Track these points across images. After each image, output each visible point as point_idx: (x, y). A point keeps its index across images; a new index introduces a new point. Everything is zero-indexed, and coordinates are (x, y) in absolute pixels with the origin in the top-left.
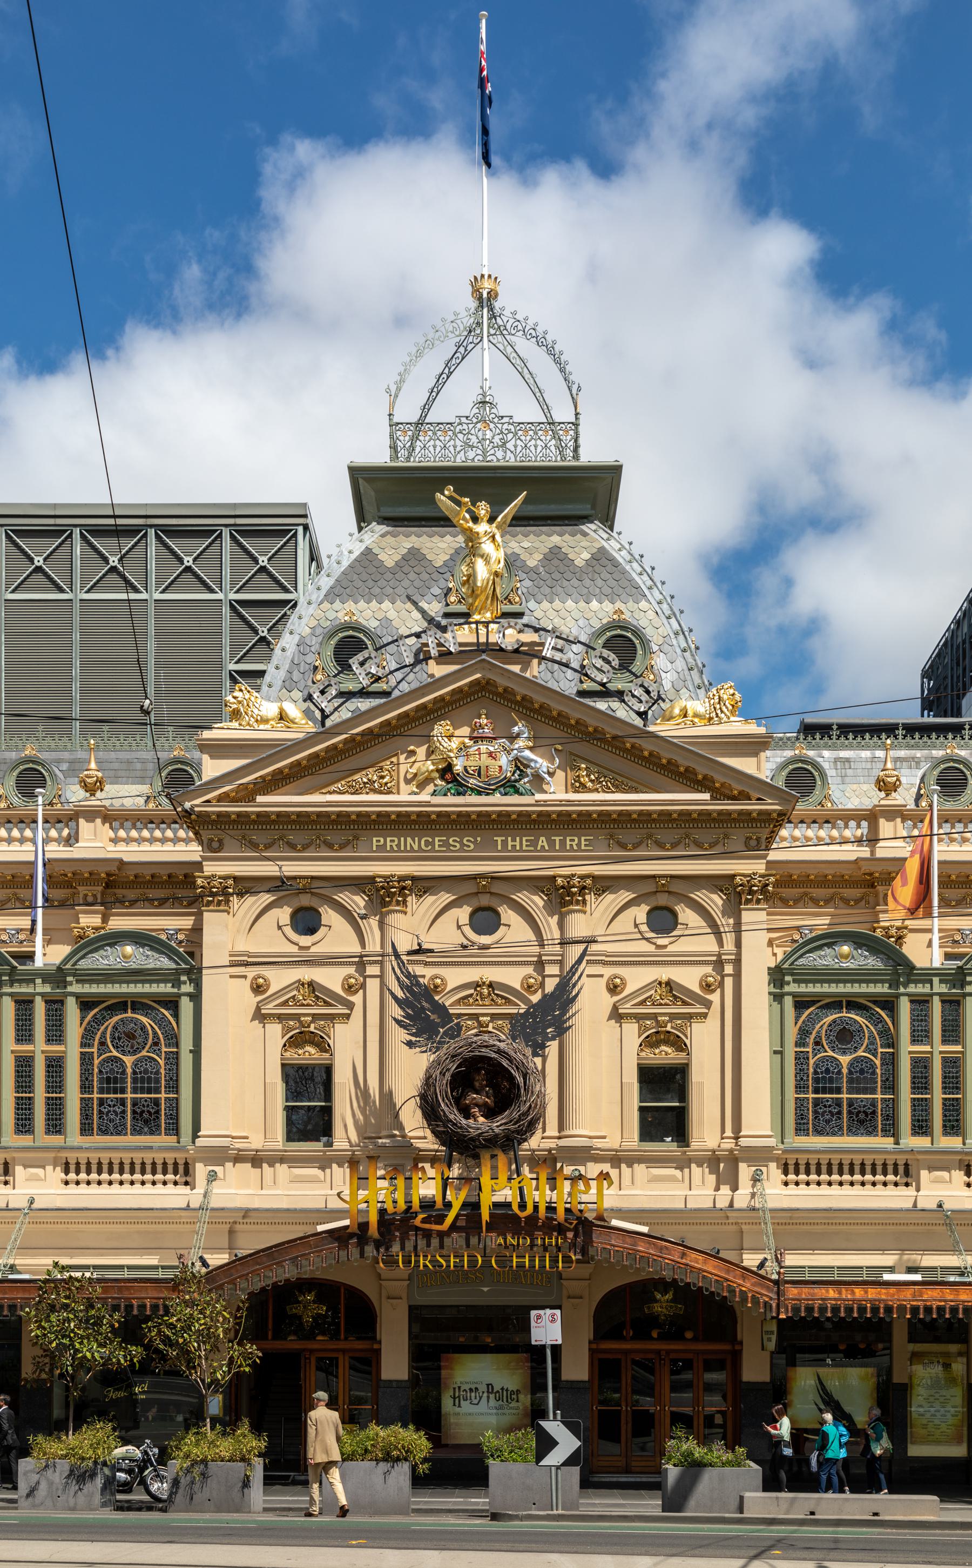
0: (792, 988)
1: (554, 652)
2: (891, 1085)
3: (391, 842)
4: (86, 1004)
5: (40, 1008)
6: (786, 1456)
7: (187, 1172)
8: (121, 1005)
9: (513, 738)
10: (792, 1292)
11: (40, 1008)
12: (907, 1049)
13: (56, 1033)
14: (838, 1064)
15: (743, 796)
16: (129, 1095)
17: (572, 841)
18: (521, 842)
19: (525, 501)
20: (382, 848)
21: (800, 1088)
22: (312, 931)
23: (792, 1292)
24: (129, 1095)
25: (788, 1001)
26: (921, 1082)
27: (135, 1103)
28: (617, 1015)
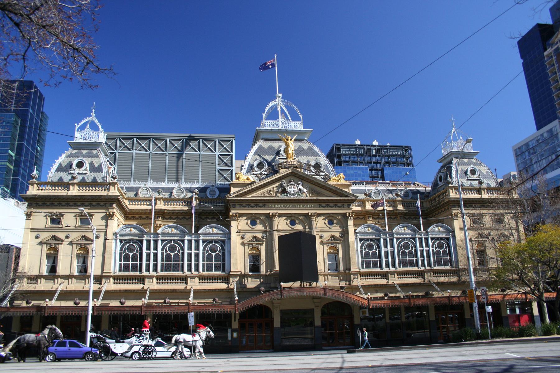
0: (359, 237)
1: (94, 175)
2: (416, 256)
3: (273, 206)
4: (204, 241)
5: (193, 242)
6: (238, 335)
7: (228, 280)
8: (211, 241)
9: (298, 184)
10: (371, 302)
11: (193, 242)
12: (419, 249)
13: (197, 248)
14: (129, 255)
15: (347, 196)
16: (131, 262)
17: (312, 206)
18: (301, 206)
19: (12, 151)
20: (271, 207)
21: (120, 260)
22: (255, 225)
23: (371, 302)
24: (214, 262)
25: (358, 239)
26: (387, 256)
27: (215, 264)
28: (243, 244)
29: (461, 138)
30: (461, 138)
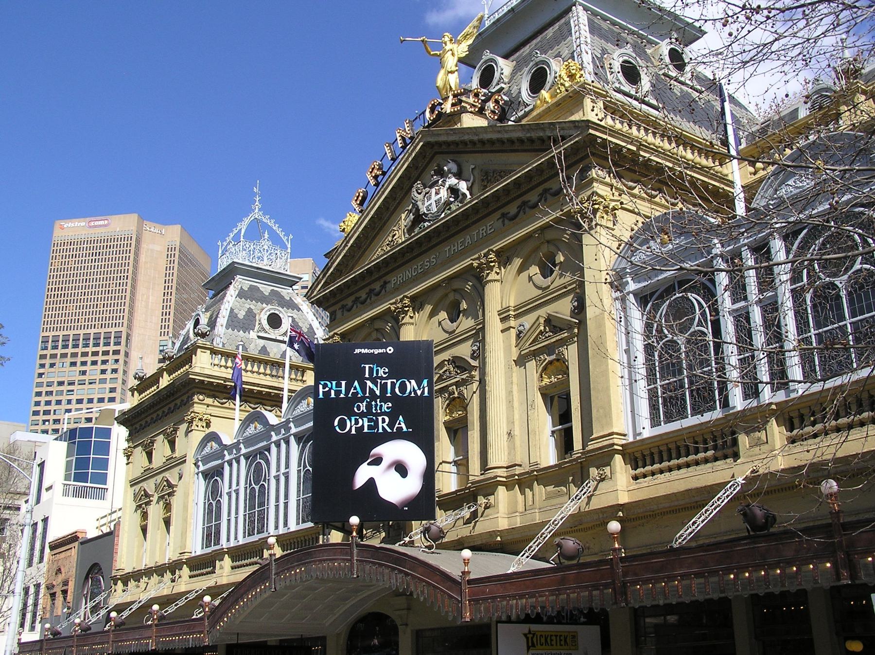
29: (266, 236)
30: (266, 236)
